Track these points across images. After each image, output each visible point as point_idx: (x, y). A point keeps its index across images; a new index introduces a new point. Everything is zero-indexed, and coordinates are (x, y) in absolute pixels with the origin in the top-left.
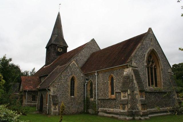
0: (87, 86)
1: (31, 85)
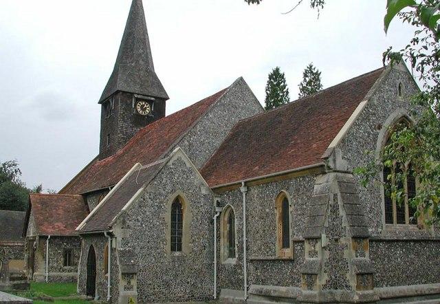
0: (218, 221)
1: (58, 220)
